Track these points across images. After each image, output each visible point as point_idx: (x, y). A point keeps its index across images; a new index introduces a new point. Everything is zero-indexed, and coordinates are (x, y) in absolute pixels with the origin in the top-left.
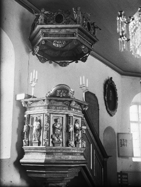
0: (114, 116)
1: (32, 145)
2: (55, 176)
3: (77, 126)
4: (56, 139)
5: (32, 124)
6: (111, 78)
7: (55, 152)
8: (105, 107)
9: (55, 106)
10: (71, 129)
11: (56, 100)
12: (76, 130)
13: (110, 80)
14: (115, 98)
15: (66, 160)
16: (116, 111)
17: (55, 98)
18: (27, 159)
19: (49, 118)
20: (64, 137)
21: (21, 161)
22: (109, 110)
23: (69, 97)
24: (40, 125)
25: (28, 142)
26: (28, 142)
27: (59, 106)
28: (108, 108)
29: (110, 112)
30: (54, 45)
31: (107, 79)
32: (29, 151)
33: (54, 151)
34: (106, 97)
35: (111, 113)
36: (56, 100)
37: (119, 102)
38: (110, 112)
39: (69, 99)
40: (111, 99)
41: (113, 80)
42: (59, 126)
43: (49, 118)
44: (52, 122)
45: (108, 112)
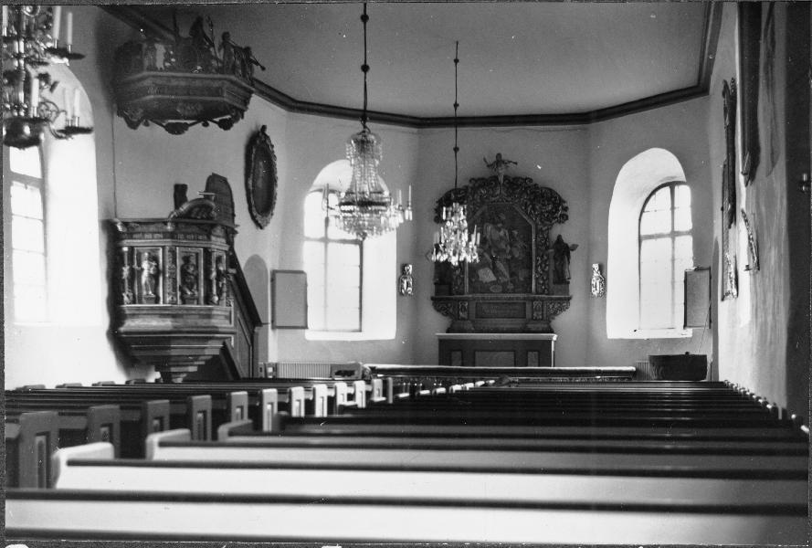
0: (266, 228)
1: (140, 303)
2: (185, 352)
3: (221, 269)
4: (189, 293)
5: (139, 264)
6: (264, 128)
7: (186, 315)
8: (246, 205)
9: (183, 233)
10: (214, 274)
11: (187, 224)
12: (220, 275)
13: (260, 134)
14: (271, 180)
15: (205, 327)
16: (272, 214)
17: (187, 220)
18: (131, 325)
19: (173, 253)
20: (202, 290)
21: (122, 329)
22: (255, 214)
23: (212, 218)
24: (157, 266)
25: (134, 296)
26: (134, 296)
27: (190, 234)
28: (254, 209)
29: (259, 218)
30: (179, 111)
31: (254, 128)
32: (137, 312)
33: (185, 312)
34: (250, 182)
35: (260, 222)
36: (187, 224)
37: (280, 190)
38: (259, 218)
39: (210, 222)
40: (260, 183)
41: (267, 132)
42: (192, 269)
43: (173, 253)
44: (179, 262)
45: (253, 218)
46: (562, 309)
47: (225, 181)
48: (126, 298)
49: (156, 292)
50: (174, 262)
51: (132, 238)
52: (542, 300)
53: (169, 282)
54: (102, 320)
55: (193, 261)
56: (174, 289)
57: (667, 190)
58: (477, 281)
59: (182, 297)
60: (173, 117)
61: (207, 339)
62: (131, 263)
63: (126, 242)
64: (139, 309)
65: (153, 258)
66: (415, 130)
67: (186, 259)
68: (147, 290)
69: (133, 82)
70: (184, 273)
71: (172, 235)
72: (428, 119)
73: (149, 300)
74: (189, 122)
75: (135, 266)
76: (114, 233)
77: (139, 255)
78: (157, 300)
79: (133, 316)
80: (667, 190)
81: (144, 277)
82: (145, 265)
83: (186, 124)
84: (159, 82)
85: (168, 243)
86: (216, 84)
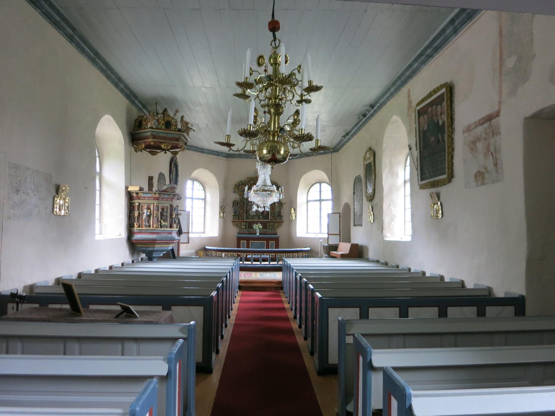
5: (142, 211)
18: (137, 237)
43: (158, 207)
44: (160, 210)
46: (280, 225)
47: (164, 175)
48: (135, 225)
49: (148, 222)
50: (158, 210)
51: (139, 199)
52: (273, 222)
53: (155, 219)
54: (123, 234)
55: (165, 210)
56: (158, 222)
57: (318, 185)
58: (249, 215)
59: (160, 225)
60: (153, 149)
61: (301, 283)
62: (139, 210)
63: (136, 201)
64: (141, 230)
65: (149, 208)
66: (225, 159)
67: (163, 209)
68: (145, 222)
69: (141, 133)
70: (162, 215)
71: (157, 199)
72: (213, 151)
73: (146, 226)
74: (159, 151)
75: (141, 212)
76: (130, 196)
77: (142, 206)
78: (149, 226)
79: (138, 233)
80: (318, 185)
81: (145, 216)
82: (145, 211)
83: (176, 152)
84: (154, 134)
85: (156, 202)
86: (177, 136)
